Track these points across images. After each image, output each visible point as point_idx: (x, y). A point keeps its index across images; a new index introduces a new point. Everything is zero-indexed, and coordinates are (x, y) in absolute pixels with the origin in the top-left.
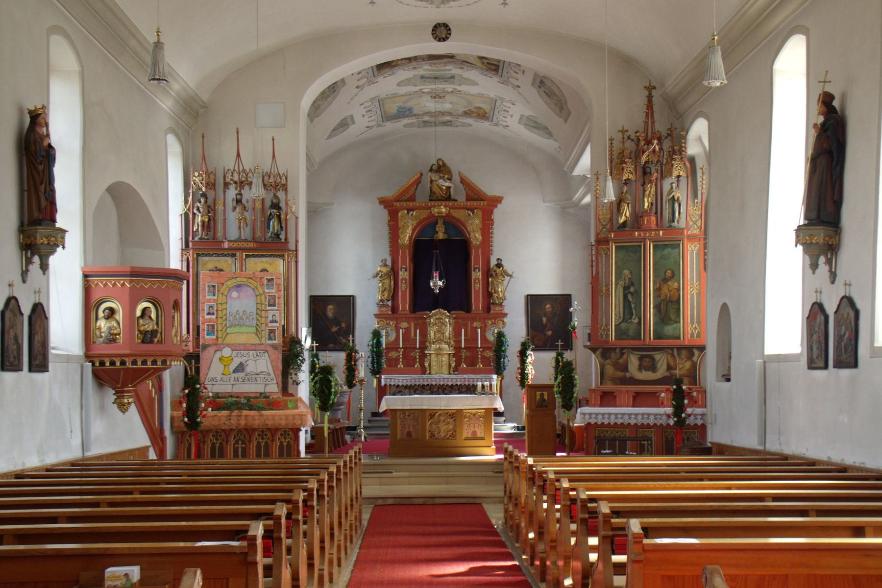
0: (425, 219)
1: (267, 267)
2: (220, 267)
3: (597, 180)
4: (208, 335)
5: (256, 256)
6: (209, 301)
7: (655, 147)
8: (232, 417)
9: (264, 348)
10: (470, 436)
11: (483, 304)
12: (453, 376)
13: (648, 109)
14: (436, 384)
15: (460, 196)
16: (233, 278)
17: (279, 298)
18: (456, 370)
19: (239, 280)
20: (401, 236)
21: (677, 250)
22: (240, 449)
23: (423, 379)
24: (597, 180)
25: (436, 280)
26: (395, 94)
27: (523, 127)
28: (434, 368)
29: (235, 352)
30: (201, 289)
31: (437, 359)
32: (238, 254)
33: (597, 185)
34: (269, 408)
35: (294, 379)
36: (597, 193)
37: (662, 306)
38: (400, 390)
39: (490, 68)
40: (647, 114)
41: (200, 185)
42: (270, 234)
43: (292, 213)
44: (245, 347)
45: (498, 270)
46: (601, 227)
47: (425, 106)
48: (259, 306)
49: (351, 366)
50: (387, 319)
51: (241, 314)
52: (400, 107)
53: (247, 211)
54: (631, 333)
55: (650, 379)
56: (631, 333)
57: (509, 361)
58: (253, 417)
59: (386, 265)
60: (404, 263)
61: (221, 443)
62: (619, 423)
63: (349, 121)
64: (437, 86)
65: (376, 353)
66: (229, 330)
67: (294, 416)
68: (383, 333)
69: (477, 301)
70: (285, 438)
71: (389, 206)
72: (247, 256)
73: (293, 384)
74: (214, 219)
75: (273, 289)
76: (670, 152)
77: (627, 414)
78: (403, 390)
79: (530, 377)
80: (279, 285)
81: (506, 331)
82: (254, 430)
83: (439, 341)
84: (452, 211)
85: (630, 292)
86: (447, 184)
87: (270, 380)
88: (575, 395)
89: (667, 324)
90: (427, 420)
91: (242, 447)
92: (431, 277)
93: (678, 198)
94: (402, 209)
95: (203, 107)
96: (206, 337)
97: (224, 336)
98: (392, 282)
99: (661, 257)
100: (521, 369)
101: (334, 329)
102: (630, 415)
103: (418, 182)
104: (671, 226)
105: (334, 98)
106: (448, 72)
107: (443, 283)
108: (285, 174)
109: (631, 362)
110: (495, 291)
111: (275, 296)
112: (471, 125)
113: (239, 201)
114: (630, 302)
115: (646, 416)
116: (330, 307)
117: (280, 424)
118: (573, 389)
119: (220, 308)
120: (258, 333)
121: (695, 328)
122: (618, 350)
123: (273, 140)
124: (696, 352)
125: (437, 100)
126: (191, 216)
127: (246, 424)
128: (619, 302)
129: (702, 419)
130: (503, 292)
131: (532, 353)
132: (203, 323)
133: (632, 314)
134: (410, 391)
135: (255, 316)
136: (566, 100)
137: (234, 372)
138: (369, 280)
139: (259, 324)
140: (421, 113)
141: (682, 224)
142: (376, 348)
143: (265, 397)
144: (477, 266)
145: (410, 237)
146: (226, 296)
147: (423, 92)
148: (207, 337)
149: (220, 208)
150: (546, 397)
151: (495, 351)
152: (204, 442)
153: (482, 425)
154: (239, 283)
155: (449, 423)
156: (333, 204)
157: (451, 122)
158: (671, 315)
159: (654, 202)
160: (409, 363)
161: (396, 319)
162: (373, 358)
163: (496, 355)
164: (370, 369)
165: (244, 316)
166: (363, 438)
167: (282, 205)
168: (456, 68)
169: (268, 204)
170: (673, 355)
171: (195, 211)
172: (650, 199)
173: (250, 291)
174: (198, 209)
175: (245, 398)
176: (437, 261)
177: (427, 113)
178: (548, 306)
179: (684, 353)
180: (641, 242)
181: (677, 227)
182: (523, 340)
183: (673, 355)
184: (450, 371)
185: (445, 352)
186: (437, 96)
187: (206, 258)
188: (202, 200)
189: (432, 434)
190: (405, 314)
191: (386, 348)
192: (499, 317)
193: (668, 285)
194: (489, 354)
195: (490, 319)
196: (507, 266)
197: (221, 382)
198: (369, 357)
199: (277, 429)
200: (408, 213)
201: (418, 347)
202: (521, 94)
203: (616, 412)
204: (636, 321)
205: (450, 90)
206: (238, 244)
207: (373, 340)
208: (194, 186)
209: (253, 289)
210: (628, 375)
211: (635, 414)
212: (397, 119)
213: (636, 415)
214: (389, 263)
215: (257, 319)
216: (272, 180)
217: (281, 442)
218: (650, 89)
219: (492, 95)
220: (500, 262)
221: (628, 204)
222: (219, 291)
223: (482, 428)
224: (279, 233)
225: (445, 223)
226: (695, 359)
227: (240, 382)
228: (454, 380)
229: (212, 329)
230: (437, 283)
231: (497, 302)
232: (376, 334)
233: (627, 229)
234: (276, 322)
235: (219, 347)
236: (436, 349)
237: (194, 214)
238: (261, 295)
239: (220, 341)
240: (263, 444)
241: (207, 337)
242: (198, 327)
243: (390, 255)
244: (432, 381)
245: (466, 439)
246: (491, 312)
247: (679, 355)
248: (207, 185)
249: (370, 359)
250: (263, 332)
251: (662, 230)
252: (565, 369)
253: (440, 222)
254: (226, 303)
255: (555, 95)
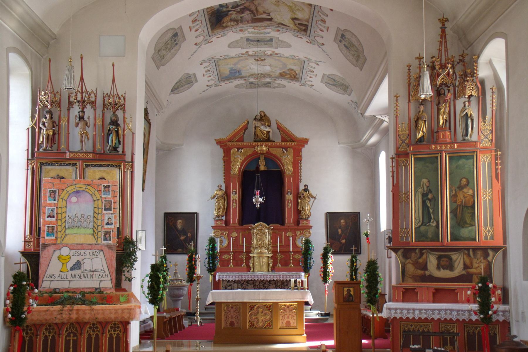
0: (250, 155)
1: (104, 175)
2: (61, 175)
3: (397, 101)
4: (48, 236)
5: (95, 166)
6: (50, 205)
7: (449, 70)
8: (64, 312)
9: (100, 248)
10: (285, 326)
11: (294, 219)
12: (271, 273)
13: (441, 38)
14: (258, 280)
15: (277, 138)
16: (72, 185)
17: (114, 203)
18: (273, 268)
19: (78, 187)
20: (233, 168)
21: (471, 161)
22: (72, 341)
23: (248, 276)
24: (397, 101)
25: (257, 197)
26: (227, 56)
27: (324, 85)
28: (257, 268)
29: (72, 251)
30: (42, 195)
31: (259, 260)
32: (78, 164)
33: (397, 105)
34: (101, 302)
35: (127, 276)
36: (396, 112)
37: (458, 210)
38: (230, 285)
39: (301, 29)
40: (441, 42)
41: (46, 103)
42: (108, 147)
43: (129, 129)
44: (82, 247)
45: (305, 194)
46: (400, 142)
47: (250, 68)
48: (96, 210)
49: (192, 265)
50: (221, 230)
51: (79, 217)
52: (232, 69)
53: (89, 127)
54: (430, 235)
55: (448, 277)
56: (430, 235)
57: (314, 262)
58: (84, 311)
59: (221, 190)
60: (234, 187)
61: (53, 336)
62: (423, 318)
63: (193, 79)
64: (259, 49)
65: (211, 255)
66: (68, 232)
67: (123, 310)
68: (218, 240)
69: (290, 217)
70: (115, 331)
71: (224, 146)
72: (87, 166)
73: (126, 280)
74: (58, 133)
75: (109, 195)
76: (462, 75)
77: (431, 310)
78: (232, 284)
79: (331, 274)
80: (115, 192)
81: (311, 239)
82: (86, 323)
83: (260, 246)
84: (270, 149)
85: (428, 199)
86: (267, 129)
87: (104, 276)
88: (379, 291)
89: (463, 227)
90: (248, 311)
91: (73, 340)
92: (253, 195)
93: (471, 115)
94: (233, 147)
95: (53, 39)
96: (45, 238)
97: (63, 237)
98: (226, 202)
99: (457, 167)
100: (324, 268)
101: (182, 238)
102: (433, 310)
103: (246, 128)
104: (464, 140)
105: (178, 50)
106: (268, 35)
107: (263, 200)
108: (124, 95)
109: (430, 261)
110: (303, 209)
111: (111, 201)
112: (285, 86)
113: (81, 118)
114: (428, 207)
115: (448, 312)
116: (180, 221)
117: (110, 318)
118: (377, 285)
119: (60, 212)
120: (95, 234)
121: (489, 231)
122: (417, 251)
123: (113, 65)
124: (491, 253)
125: (259, 62)
126: (37, 130)
127: (77, 318)
128: (418, 207)
129: (503, 315)
130: (309, 210)
131: (332, 255)
132: (44, 225)
133: (430, 218)
134: (238, 285)
135: (92, 219)
136: (363, 48)
137: (72, 269)
138: (208, 200)
139: (96, 227)
140: (248, 75)
141: (474, 138)
142: (212, 252)
143: (99, 292)
144: (290, 190)
145: (240, 169)
146: (66, 201)
147: (249, 55)
148: (46, 238)
149: (64, 123)
150: (352, 293)
151: (304, 254)
152: (37, 335)
153: (295, 316)
154: (78, 189)
155: (266, 314)
156: (182, 145)
157: (270, 83)
158: (467, 219)
159: (448, 120)
160: (238, 263)
161: (228, 230)
162: (209, 259)
163: (304, 257)
164: (207, 268)
165: (82, 219)
166: (199, 323)
167: (120, 122)
168: (274, 30)
169: (108, 120)
170: (469, 255)
171: (41, 126)
172: (445, 116)
173: (88, 197)
174: (44, 124)
175: (80, 293)
176: (258, 182)
177: (252, 75)
178: (342, 221)
179: (479, 253)
180: (438, 154)
181: (471, 141)
182: (325, 246)
183: (469, 255)
184: (268, 269)
185: (265, 255)
186: (259, 59)
187: (49, 167)
188: (48, 116)
189: (251, 323)
190: (235, 226)
191: (220, 252)
192: (306, 229)
193: (463, 192)
194: (299, 257)
195: (299, 230)
196: (312, 191)
197: (59, 279)
198: (206, 259)
199: (107, 323)
200: (238, 150)
201: (244, 251)
202: (324, 52)
203: (421, 308)
204: (434, 224)
205: (269, 53)
206: (79, 155)
207: (209, 245)
208: (40, 103)
209: (91, 195)
210: (427, 273)
211: (438, 310)
212: (229, 80)
213: (440, 310)
214: (223, 188)
215: (94, 222)
216: (111, 100)
217: (111, 335)
218: (444, 21)
219: (301, 57)
220: (307, 187)
221: (425, 121)
222: (59, 196)
223: (295, 318)
224: (117, 146)
225: (265, 158)
226: (490, 258)
227: (76, 279)
228: (272, 277)
229: (52, 230)
230: (258, 200)
231: (305, 218)
232: (212, 241)
233: (424, 143)
234: (112, 224)
235: (57, 246)
236: (258, 253)
237: (40, 129)
238: (98, 200)
239: (59, 241)
240: (94, 337)
241: (46, 238)
242: (39, 229)
243: (224, 182)
244: (255, 277)
245: (281, 328)
246: (300, 225)
247: (474, 255)
248: (52, 103)
249: (207, 260)
250: (100, 233)
251: (457, 143)
252: (370, 268)
253: (262, 158)
254: (66, 207)
255: (353, 46)
